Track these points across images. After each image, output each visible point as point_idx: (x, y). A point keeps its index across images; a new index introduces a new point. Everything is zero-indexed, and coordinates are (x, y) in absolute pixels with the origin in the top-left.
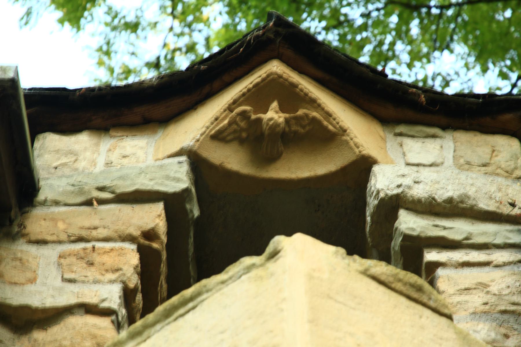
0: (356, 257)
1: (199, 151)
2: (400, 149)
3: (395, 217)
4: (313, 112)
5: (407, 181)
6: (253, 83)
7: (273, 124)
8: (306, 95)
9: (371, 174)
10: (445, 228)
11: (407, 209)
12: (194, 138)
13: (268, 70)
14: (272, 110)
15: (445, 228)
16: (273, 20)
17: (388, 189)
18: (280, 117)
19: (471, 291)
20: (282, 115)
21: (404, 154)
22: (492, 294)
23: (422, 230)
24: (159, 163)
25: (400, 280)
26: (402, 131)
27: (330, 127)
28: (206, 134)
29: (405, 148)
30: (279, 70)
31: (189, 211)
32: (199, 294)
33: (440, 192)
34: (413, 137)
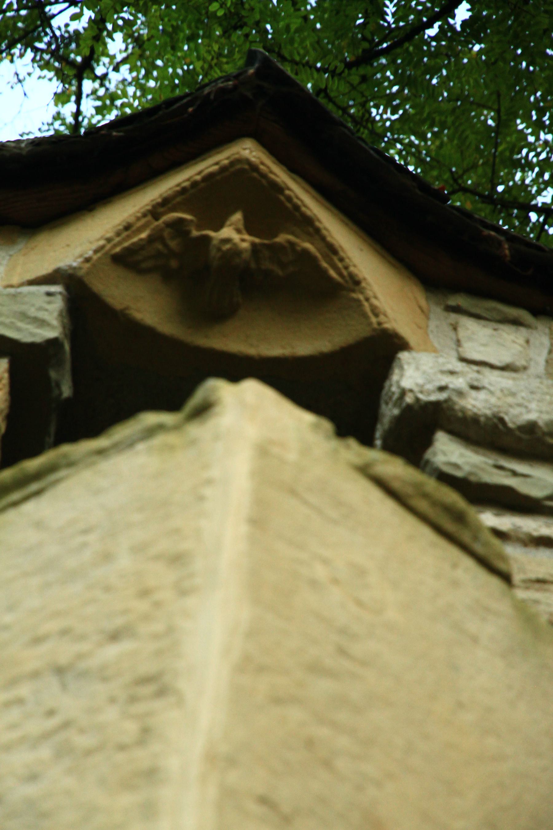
0: (353, 443)
1: (86, 279)
2: (452, 334)
3: (428, 442)
4: (304, 241)
5: (459, 383)
6: (203, 174)
7: (228, 250)
8: (297, 208)
9: (395, 364)
10: (515, 474)
11: (451, 432)
12: (81, 256)
13: (233, 154)
14: (230, 225)
15: (515, 474)
16: (257, 65)
17: (421, 392)
18: (243, 240)
19: (546, 586)
20: (247, 237)
21: (458, 343)
23: (474, 470)
24: (12, 291)
25: (426, 496)
26: (460, 304)
27: (332, 273)
28: (103, 252)
29: (462, 333)
30: (254, 157)
31: (53, 384)
32: (52, 468)
33: (515, 411)
34: (477, 317)
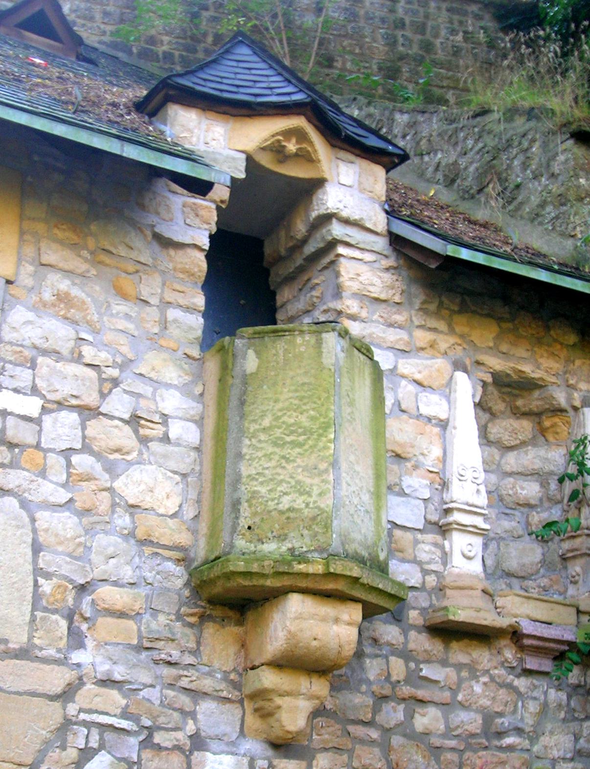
22: (422, 349)
